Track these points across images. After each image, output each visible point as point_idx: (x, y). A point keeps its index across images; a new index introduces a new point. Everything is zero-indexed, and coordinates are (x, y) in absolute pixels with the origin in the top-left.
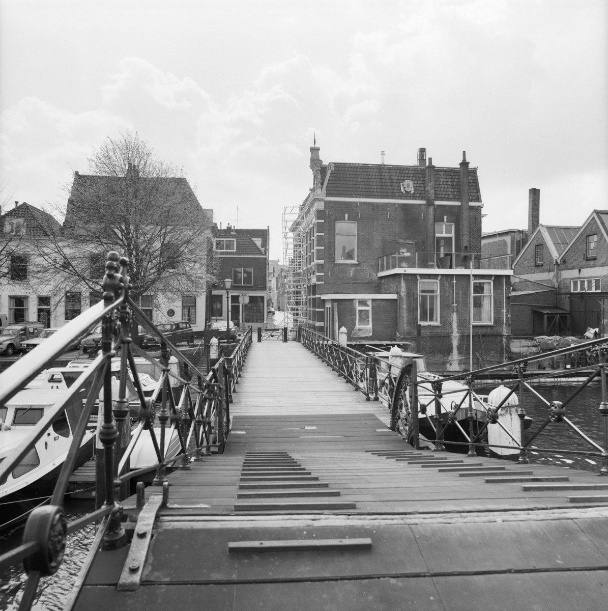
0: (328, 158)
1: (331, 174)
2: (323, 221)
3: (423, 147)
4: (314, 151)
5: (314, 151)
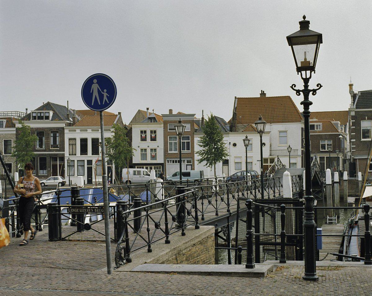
0: (356, 90)
1: (359, 97)
2: (354, 121)
3: (145, 130)
4: (351, 86)
5: (351, 86)
